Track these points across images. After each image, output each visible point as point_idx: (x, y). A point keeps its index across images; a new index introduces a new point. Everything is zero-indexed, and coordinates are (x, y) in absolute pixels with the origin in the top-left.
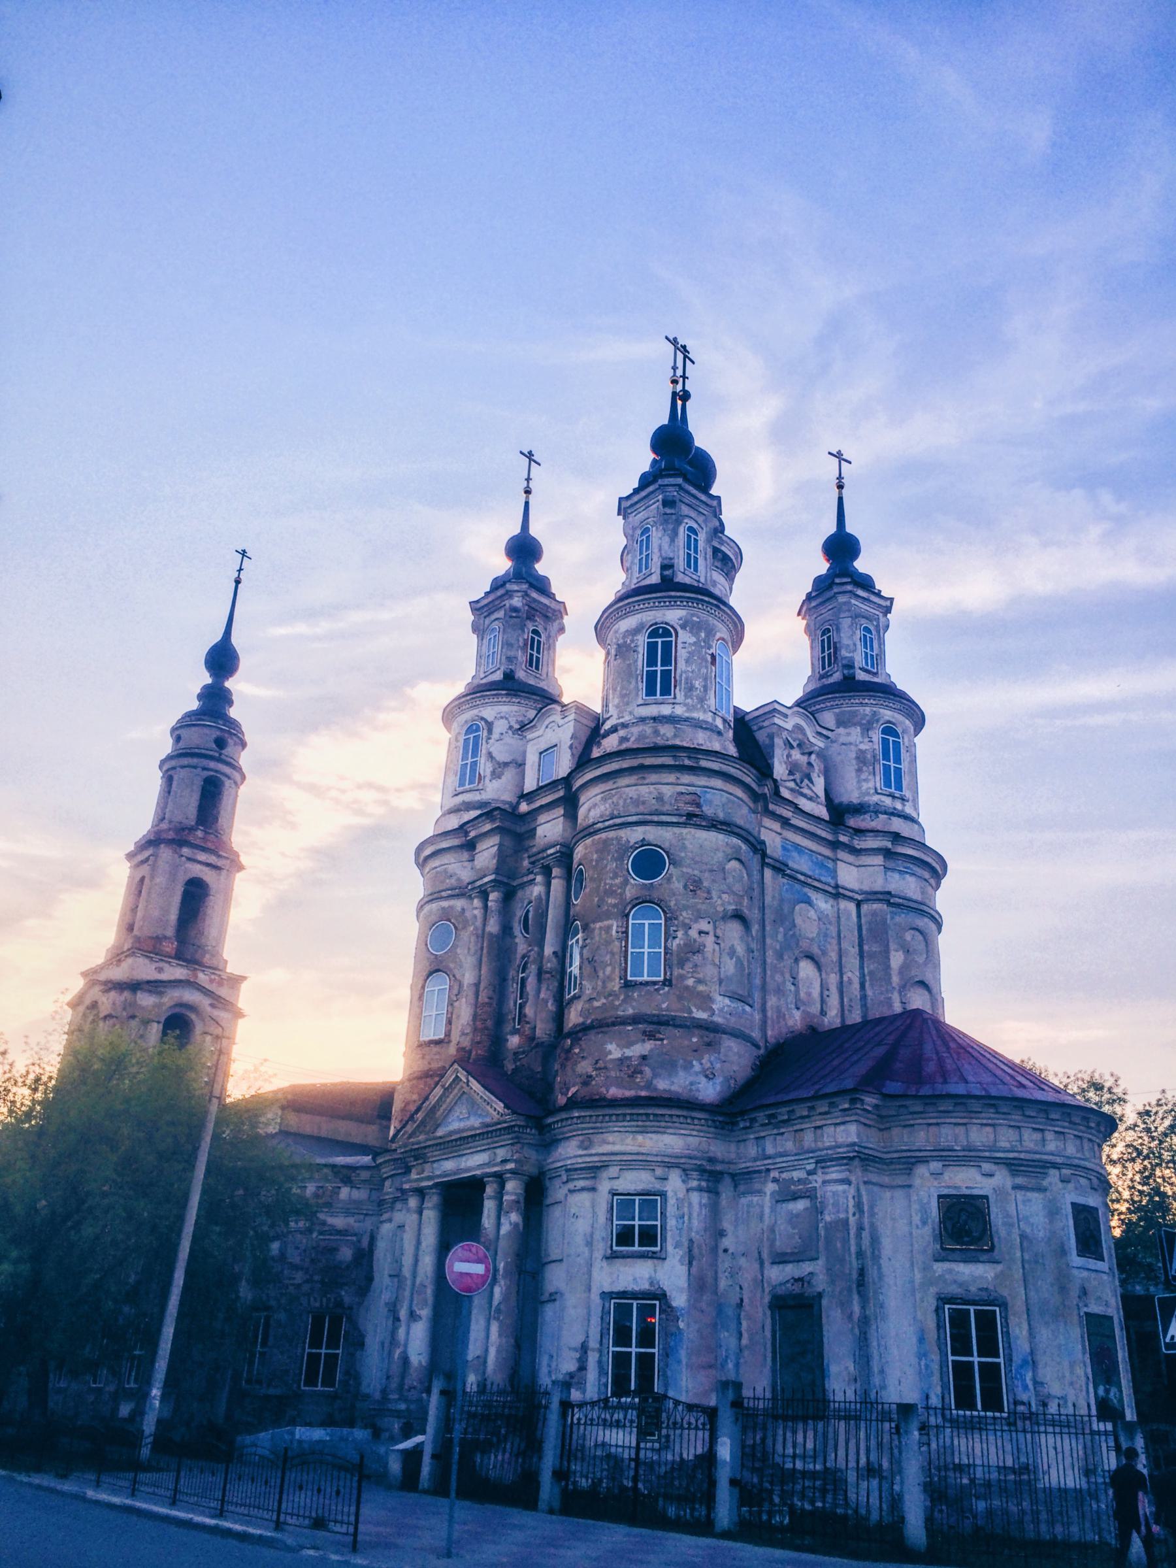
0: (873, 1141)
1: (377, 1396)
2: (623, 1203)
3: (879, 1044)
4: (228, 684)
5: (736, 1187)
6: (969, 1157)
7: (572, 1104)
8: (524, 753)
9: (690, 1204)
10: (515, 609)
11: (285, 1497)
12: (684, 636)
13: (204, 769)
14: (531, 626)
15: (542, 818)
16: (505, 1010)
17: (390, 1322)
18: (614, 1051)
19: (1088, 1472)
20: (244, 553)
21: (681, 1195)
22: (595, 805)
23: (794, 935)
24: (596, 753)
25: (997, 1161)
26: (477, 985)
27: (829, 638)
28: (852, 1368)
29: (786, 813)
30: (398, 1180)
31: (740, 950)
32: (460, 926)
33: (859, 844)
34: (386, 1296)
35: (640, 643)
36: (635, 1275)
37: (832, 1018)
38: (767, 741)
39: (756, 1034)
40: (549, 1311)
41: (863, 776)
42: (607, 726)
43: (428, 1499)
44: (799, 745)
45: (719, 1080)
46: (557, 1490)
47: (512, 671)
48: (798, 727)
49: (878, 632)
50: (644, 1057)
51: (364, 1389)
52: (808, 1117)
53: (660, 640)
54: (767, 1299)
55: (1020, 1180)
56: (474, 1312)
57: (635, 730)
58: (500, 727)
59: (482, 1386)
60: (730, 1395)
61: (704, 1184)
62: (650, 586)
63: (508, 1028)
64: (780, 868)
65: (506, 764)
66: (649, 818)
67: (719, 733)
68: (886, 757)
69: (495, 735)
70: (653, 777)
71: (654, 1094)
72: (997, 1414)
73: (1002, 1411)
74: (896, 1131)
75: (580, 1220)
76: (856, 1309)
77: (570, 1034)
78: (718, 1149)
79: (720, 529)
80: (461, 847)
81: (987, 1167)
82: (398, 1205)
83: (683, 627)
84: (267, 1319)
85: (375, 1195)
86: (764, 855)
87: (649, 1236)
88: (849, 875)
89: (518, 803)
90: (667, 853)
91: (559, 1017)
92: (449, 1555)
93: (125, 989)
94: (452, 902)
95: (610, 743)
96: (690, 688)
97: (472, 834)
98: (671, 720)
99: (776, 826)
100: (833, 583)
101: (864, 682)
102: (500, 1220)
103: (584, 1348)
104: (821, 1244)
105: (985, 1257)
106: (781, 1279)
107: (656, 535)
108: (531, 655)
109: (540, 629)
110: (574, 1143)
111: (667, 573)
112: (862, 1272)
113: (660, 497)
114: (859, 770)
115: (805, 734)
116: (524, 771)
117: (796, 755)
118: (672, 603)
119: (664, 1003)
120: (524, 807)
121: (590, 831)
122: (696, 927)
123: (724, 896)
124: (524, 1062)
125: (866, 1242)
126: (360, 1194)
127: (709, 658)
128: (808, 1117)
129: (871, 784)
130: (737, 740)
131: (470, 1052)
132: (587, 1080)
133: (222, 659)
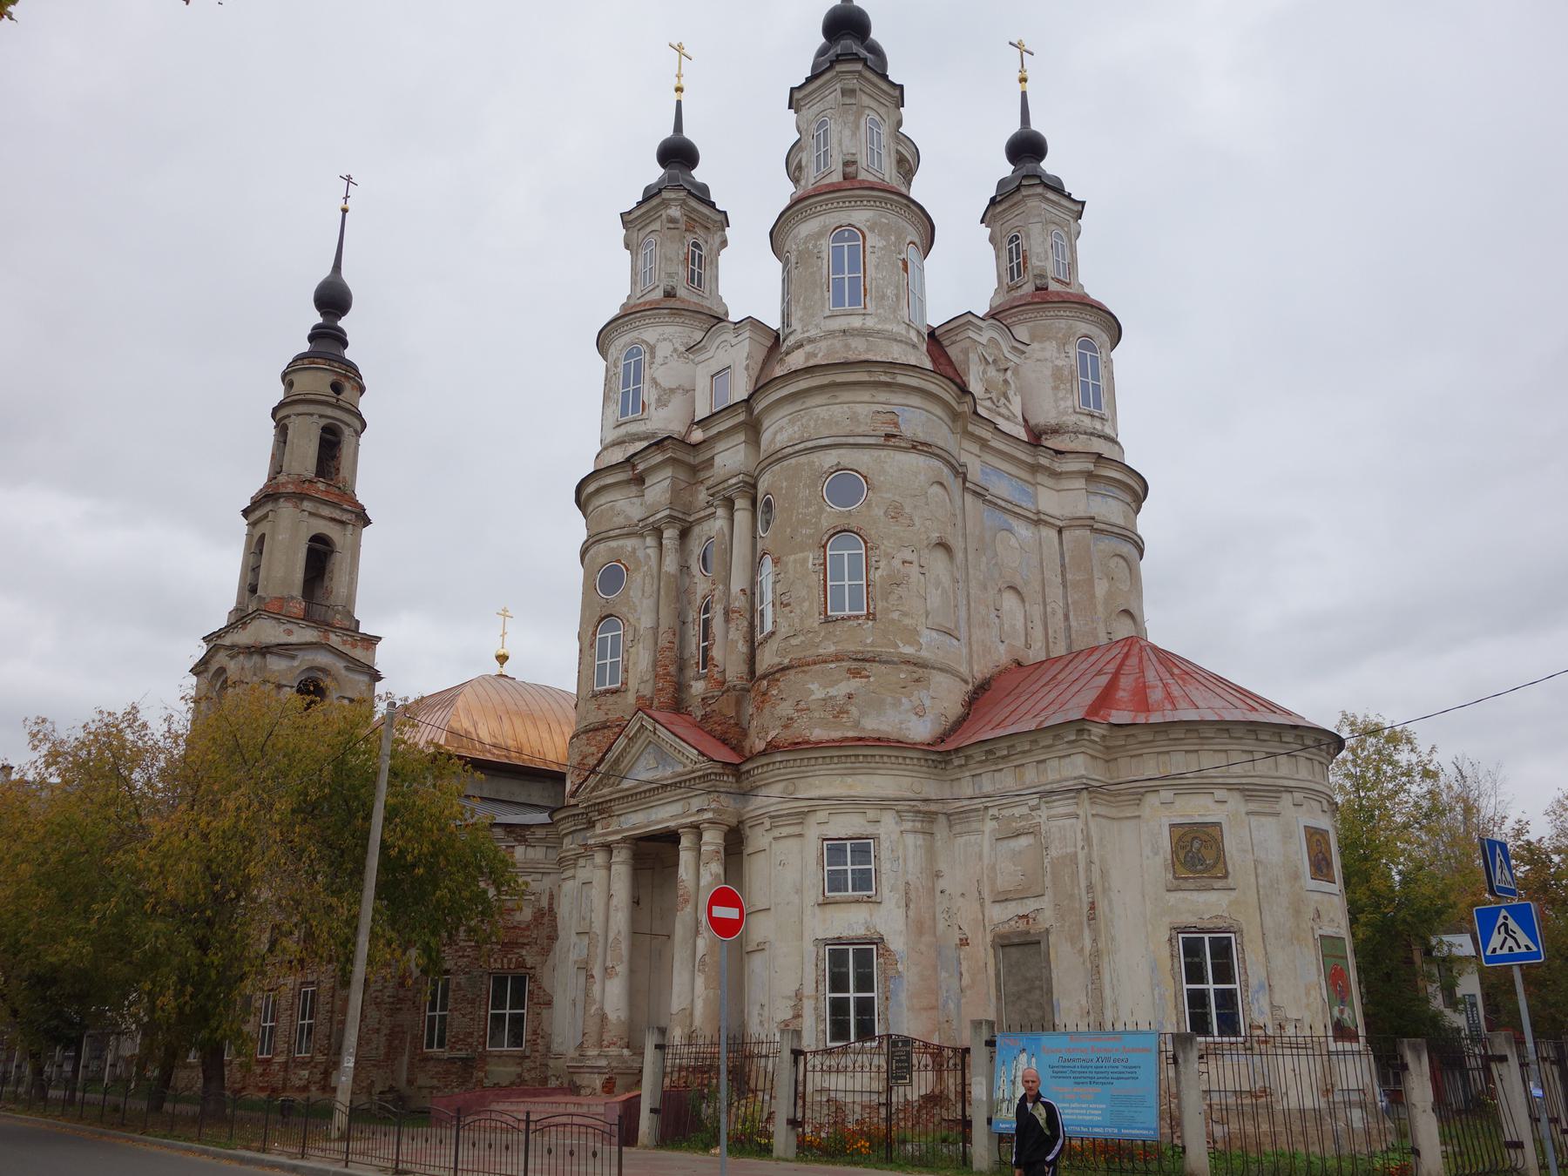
0: (1097, 774)
1: (572, 1053)
2: (835, 850)
3: (1100, 673)
4: (342, 323)
6: (1200, 785)
7: (772, 748)
8: (694, 379)
9: (905, 847)
10: (672, 220)
12: (872, 240)
13: (321, 416)
14: (690, 238)
15: (720, 446)
17: (582, 979)
18: (817, 691)
19: (1328, 1091)
20: (349, 179)
24: (779, 371)
25: (1230, 788)
26: (655, 629)
28: (1084, 1002)
30: (579, 838)
31: (946, 581)
32: (631, 567)
34: (573, 956)
36: (850, 921)
37: (1036, 654)
39: (963, 669)
40: (756, 963)
41: (1061, 395)
42: (791, 341)
44: (995, 361)
45: (929, 717)
46: (793, 1141)
48: (992, 339)
50: (850, 696)
51: (556, 1047)
52: (1030, 751)
54: (989, 939)
55: (1253, 806)
56: (677, 965)
57: (823, 344)
58: (663, 350)
59: (690, 1039)
60: (985, 1036)
61: (918, 825)
62: (650, 302)
63: (691, 672)
65: (672, 391)
66: (844, 440)
67: (914, 346)
69: (659, 360)
70: (846, 396)
71: (862, 735)
72: (1233, 1039)
73: (1236, 1033)
74: (1122, 762)
75: (785, 870)
76: (1088, 943)
77: (764, 677)
78: (931, 789)
80: (628, 482)
81: (1220, 794)
82: (582, 862)
83: (871, 229)
85: (553, 855)
86: (965, 480)
87: (863, 880)
88: (1052, 500)
89: (689, 431)
91: (751, 660)
93: (251, 654)
94: (621, 542)
95: (796, 360)
96: (883, 297)
97: (641, 467)
98: (863, 333)
99: (975, 448)
100: (1018, 188)
101: (1058, 293)
102: (698, 872)
103: (799, 996)
104: (1048, 879)
105: (1219, 884)
106: (1004, 918)
107: (834, 127)
109: (700, 242)
110: (776, 790)
111: (849, 170)
112: (1092, 906)
114: (1056, 388)
117: (992, 372)
118: (858, 203)
119: (867, 638)
120: (697, 436)
121: (777, 457)
122: (900, 556)
124: (714, 707)
125: (1096, 877)
126: (537, 853)
128: (1030, 751)
129: (1069, 403)
131: (652, 699)
132: (788, 723)
133: (333, 299)
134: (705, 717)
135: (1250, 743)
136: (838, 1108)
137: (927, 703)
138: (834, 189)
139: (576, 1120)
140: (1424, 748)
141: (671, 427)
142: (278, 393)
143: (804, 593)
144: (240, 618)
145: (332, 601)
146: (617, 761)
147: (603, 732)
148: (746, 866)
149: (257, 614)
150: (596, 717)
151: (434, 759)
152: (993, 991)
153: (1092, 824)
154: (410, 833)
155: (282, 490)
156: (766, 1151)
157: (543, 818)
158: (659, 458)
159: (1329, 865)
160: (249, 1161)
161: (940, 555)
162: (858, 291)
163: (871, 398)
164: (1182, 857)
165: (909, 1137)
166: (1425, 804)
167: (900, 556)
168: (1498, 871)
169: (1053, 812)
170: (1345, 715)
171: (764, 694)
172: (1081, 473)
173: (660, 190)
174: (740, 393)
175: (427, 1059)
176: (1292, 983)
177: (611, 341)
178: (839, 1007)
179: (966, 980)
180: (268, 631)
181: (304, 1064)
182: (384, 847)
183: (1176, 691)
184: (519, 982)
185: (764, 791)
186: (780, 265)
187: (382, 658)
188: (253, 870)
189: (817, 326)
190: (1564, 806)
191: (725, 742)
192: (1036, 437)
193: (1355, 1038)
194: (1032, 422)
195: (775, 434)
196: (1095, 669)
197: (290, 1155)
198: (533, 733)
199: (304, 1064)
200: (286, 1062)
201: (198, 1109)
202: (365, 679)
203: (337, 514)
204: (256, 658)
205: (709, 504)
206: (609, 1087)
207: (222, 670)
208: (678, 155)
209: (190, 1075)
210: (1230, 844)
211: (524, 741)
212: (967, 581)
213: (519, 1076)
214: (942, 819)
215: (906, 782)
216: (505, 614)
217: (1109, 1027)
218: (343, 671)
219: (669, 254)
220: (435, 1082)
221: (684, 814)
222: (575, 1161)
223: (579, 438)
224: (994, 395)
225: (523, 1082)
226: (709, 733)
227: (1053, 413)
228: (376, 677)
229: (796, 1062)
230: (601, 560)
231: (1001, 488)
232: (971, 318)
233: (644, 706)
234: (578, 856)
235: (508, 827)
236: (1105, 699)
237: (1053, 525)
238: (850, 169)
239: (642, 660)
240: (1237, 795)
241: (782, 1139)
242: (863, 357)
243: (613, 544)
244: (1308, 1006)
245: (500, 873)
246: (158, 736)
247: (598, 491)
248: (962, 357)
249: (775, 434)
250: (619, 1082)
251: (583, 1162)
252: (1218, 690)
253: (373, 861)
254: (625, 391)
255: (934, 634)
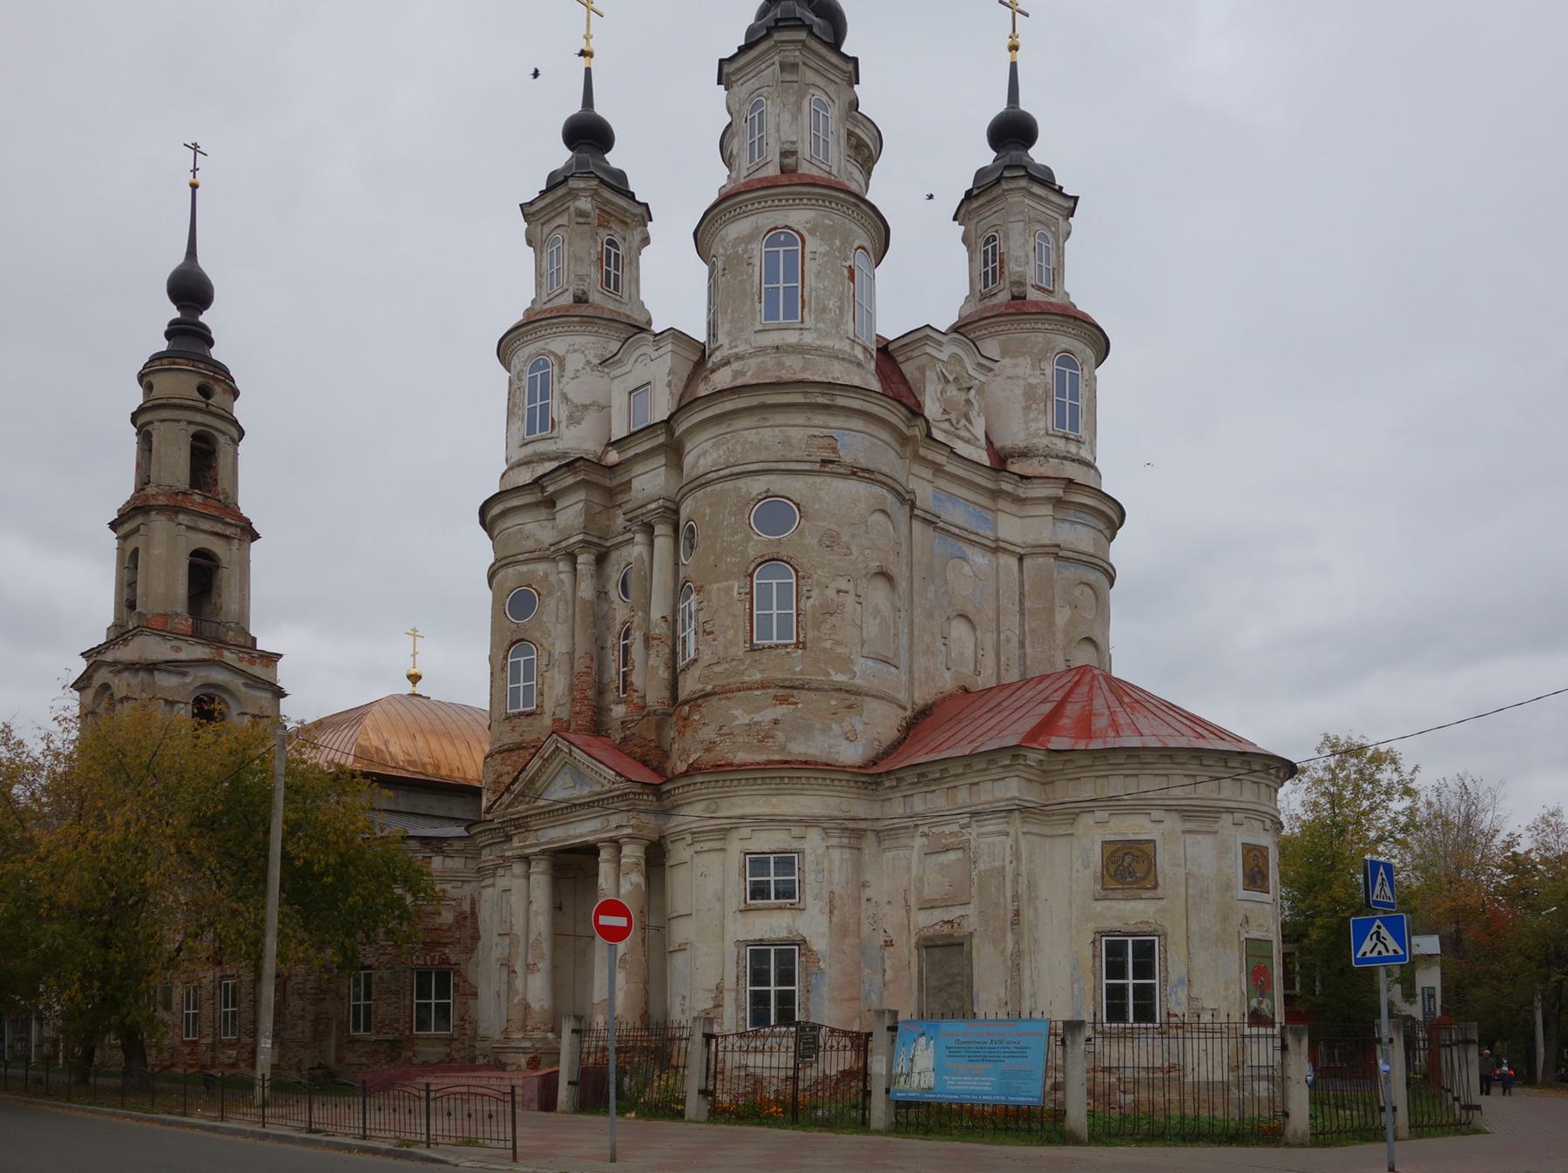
0: (1033, 796)
1: (498, 1036)
2: (758, 863)
4: (205, 318)
5: (879, 842)
6: (1140, 807)
9: (831, 860)
10: (581, 213)
11: (432, 1122)
12: (812, 244)
13: (189, 423)
15: (639, 469)
16: (606, 679)
17: (505, 975)
18: (741, 716)
20: (195, 147)
21: (820, 851)
22: (705, 452)
23: (946, 592)
24: (703, 390)
25: (1168, 809)
27: (994, 248)
28: (1002, 995)
29: (940, 458)
30: (497, 850)
31: (886, 609)
32: (543, 592)
33: (1025, 491)
34: (496, 953)
35: (756, 252)
36: (772, 925)
37: (986, 679)
38: (917, 375)
39: (902, 696)
40: (679, 961)
41: (1032, 416)
42: (717, 357)
43: (287, 1121)
44: (956, 379)
47: (584, 292)
48: (953, 356)
49: (1057, 241)
50: (776, 722)
53: (781, 249)
54: (913, 941)
55: (1190, 826)
57: (753, 362)
58: (574, 362)
60: (887, 1022)
61: (845, 841)
62: (558, 309)
63: (611, 696)
64: (930, 522)
65: (585, 407)
66: (775, 466)
67: (859, 365)
68: (1061, 393)
69: (569, 372)
70: (778, 418)
73: (1153, 1020)
75: (708, 885)
76: (1010, 944)
77: (686, 702)
78: (859, 808)
79: (854, 104)
80: (537, 504)
81: (1156, 814)
82: (500, 872)
83: (812, 232)
84: (368, 978)
85: (472, 864)
86: (913, 506)
87: (786, 892)
89: (605, 452)
90: (797, 505)
91: (674, 686)
92: (613, 1160)
93: (137, 670)
94: (531, 567)
95: (722, 379)
96: (824, 309)
97: (550, 489)
98: (799, 349)
100: (998, 181)
101: (1036, 303)
103: (720, 989)
104: (974, 891)
105: (1149, 894)
106: (929, 922)
107: (770, 109)
108: (608, 273)
109: (617, 239)
110: (697, 809)
112: (1017, 913)
113: (776, 59)
114: (1027, 408)
115: (964, 367)
116: (609, 414)
117: (952, 391)
118: (796, 201)
119: (797, 666)
120: (613, 457)
121: (699, 483)
122: (834, 585)
123: (867, 552)
124: (634, 730)
126: (456, 863)
127: (846, 272)
128: (941, 778)
129: (1041, 425)
130: (880, 372)
132: (710, 747)
133: (190, 290)
134: (624, 739)
135: (1193, 768)
136: (758, 1081)
137: (860, 728)
138: (769, 184)
139: (472, 1090)
140: (1406, 768)
141: (585, 446)
142: (136, 397)
143: (728, 621)
144: (120, 634)
145: (223, 618)
146: (532, 781)
147: (518, 751)
148: (668, 876)
149: (139, 630)
150: (510, 738)
151: (336, 778)
152: (915, 986)
153: (1023, 842)
154: (314, 845)
155: (152, 502)
156: (680, 1115)
157: (460, 831)
158: (570, 480)
159: (1265, 877)
160: (170, 1123)
161: (880, 585)
162: (795, 303)
163: (813, 415)
164: (1112, 870)
165: (820, 1102)
166: (1403, 819)
167: (834, 585)
168: (1378, 888)
169: (983, 830)
170: (1327, 738)
171: (686, 719)
172: (1048, 499)
173: (566, 179)
174: (661, 412)
175: (354, 1041)
176: (1210, 977)
177: (514, 352)
178: (760, 1000)
179: (889, 975)
180: (154, 648)
181: (231, 1045)
182: (286, 857)
183: (1122, 719)
184: (443, 979)
185: (685, 810)
186: (705, 268)
187: (284, 675)
188: (149, 878)
189: (746, 341)
190: (1550, 821)
191: (645, 763)
192: (1000, 460)
193: (1272, 1024)
194: (997, 445)
195: (699, 457)
196: (1044, 696)
197: (210, 1118)
198: (450, 750)
199: (231, 1045)
200: (213, 1044)
201: (119, 1081)
202: (269, 695)
203: (219, 528)
204: (142, 675)
205: (627, 530)
206: (534, 1063)
207: (105, 687)
208: (588, 134)
209: (110, 1050)
210: (1162, 859)
211: (441, 757)
212: (911, 610)
213: (448, 1055)
214: (871, 836)
215: (833, 802)
216: (414, 633)
217: (1025, 1015)
218: (242, 688)
219: (579, 253)
220: (364, 1060)
221: (603, 830)
222: (494, 1123)
223: (483, 456)
224: (953, 417)
225: (452, 1060)
226: (629, 755)
227: (1022, 435)
228: (280, 693)
229: (708, 1044)
230: (510, 585)
231: (956, 515)
232: (929, 332)
233: (560, 728)
234: (497, 867)
235: (425, 841)
236: (1047, 725)
237: (1012, 553)
238: (790, 161)
239: (557, 684)
240: (1174, 815)
241: (694, 1105)
242: (799, 376)
243: (523, 568)
244: (1226, 998)
245: (414, 880)
246: (36, 753)
247: (504, 513)
248: (917, 375)
249: (699, 457)
250: (544, 1060)
251: (501, 1124)
252: (1168, 719)
253: (275, 872)
254: (531, 407)
255: (870, 662)
